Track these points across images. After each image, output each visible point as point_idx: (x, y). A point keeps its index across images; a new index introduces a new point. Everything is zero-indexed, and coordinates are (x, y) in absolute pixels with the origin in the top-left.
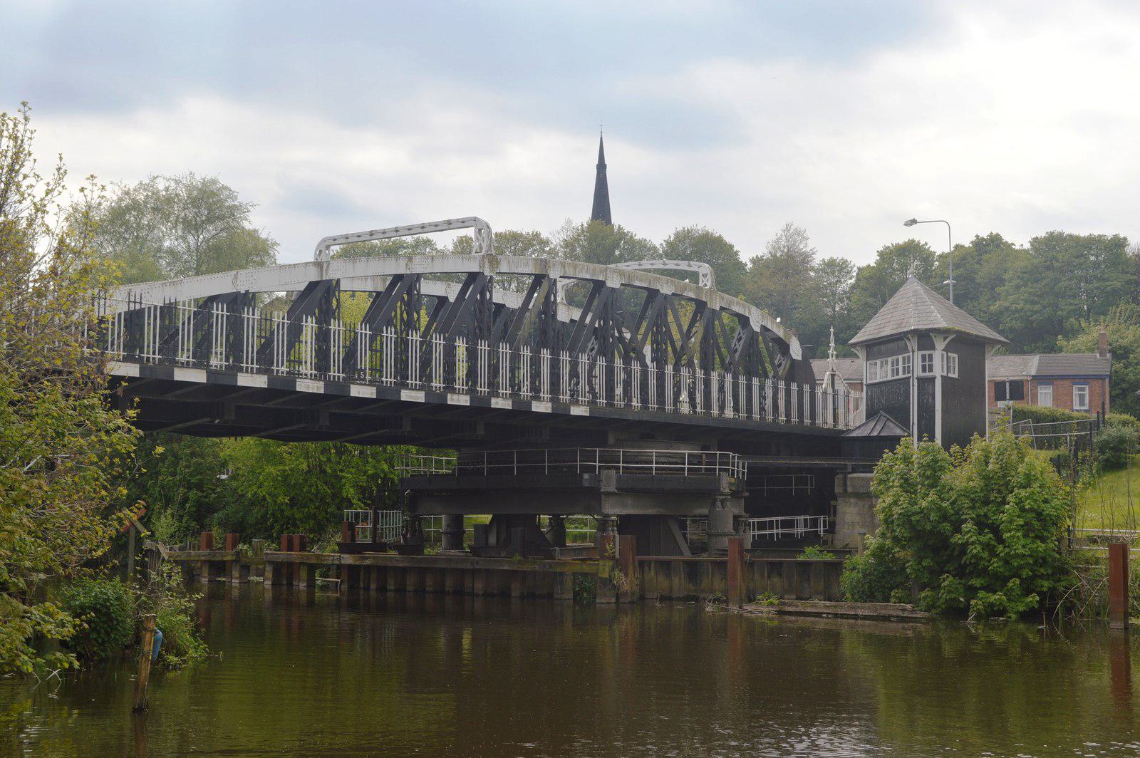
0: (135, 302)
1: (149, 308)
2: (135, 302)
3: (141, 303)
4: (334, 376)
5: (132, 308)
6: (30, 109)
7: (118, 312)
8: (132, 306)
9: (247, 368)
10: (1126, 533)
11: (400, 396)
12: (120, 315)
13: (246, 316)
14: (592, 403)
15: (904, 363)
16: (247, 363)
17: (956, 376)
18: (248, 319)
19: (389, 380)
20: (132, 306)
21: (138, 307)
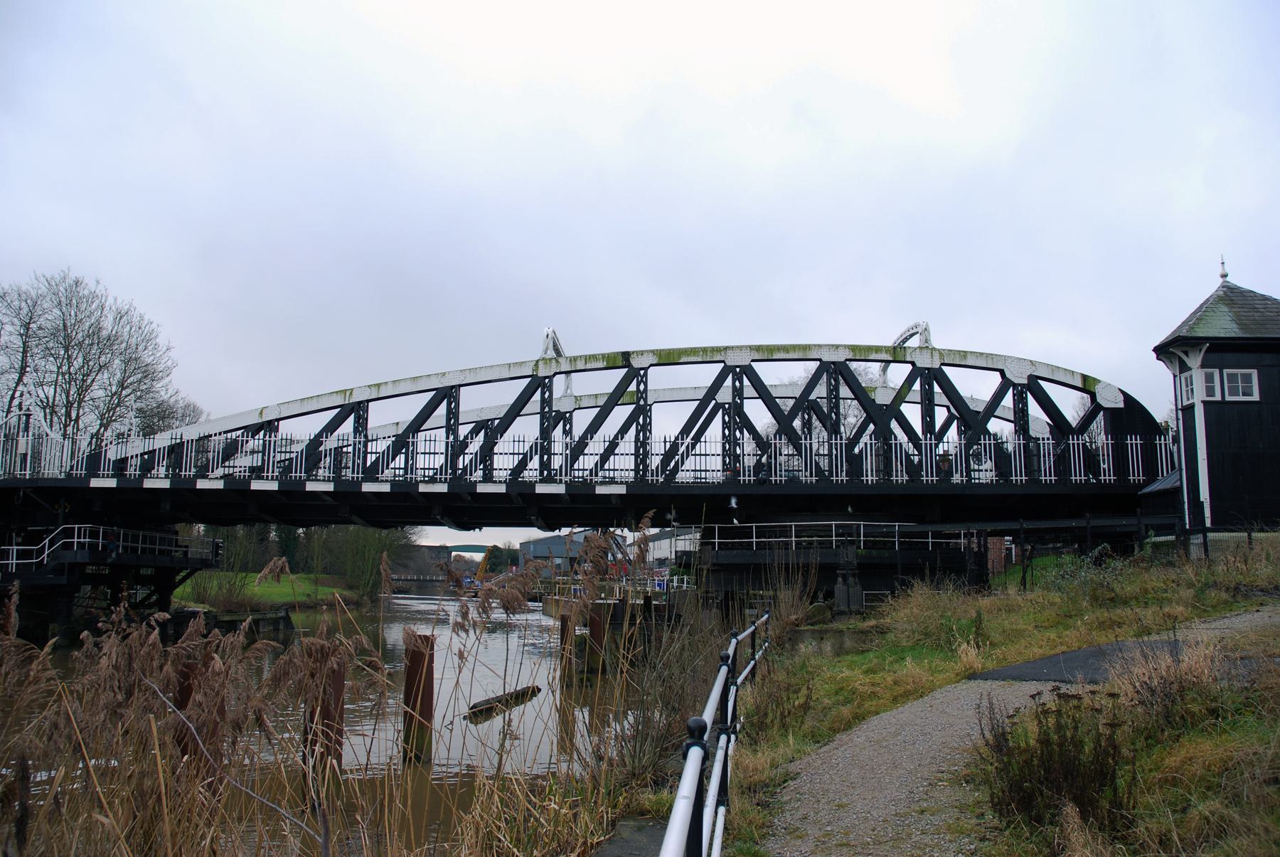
0: (343, 440)
1: (188, 441)
2: (343, 440)
3: (181, 438)
4: (130, 475)
5: (174, 441)
6: (98, 282)
7: (328, 448)
8: (174, 441)
9: (103, 474)
10: (398, 580)
11: (196, 485)
12: (164, 448)
13: (1129, 442)
14: (337, 479)
15: (1187, 386)
16: (1134, 476)
17: (1256, 397)
18: (1132, 444)
19: (1019, 478)
20: (174, 441)
21: (178, 441)
